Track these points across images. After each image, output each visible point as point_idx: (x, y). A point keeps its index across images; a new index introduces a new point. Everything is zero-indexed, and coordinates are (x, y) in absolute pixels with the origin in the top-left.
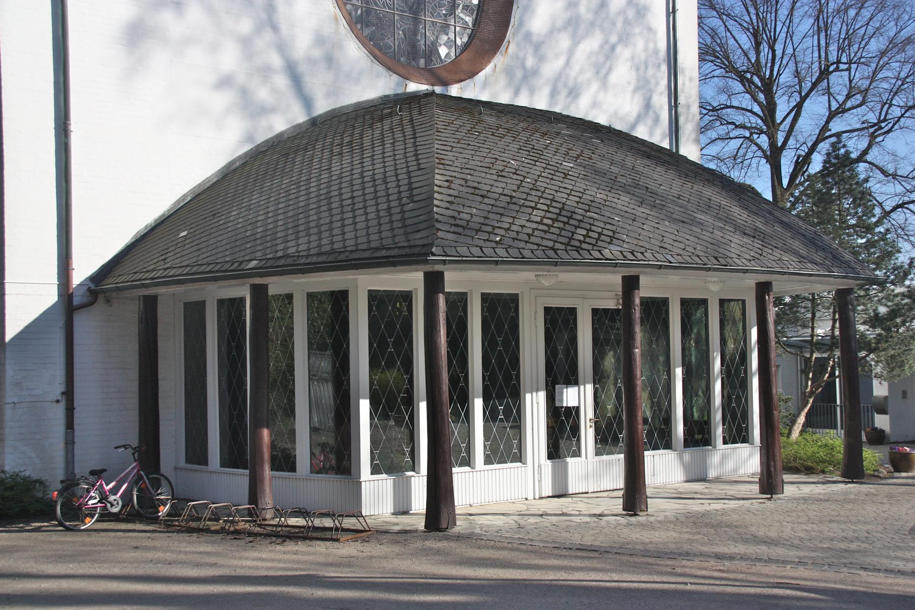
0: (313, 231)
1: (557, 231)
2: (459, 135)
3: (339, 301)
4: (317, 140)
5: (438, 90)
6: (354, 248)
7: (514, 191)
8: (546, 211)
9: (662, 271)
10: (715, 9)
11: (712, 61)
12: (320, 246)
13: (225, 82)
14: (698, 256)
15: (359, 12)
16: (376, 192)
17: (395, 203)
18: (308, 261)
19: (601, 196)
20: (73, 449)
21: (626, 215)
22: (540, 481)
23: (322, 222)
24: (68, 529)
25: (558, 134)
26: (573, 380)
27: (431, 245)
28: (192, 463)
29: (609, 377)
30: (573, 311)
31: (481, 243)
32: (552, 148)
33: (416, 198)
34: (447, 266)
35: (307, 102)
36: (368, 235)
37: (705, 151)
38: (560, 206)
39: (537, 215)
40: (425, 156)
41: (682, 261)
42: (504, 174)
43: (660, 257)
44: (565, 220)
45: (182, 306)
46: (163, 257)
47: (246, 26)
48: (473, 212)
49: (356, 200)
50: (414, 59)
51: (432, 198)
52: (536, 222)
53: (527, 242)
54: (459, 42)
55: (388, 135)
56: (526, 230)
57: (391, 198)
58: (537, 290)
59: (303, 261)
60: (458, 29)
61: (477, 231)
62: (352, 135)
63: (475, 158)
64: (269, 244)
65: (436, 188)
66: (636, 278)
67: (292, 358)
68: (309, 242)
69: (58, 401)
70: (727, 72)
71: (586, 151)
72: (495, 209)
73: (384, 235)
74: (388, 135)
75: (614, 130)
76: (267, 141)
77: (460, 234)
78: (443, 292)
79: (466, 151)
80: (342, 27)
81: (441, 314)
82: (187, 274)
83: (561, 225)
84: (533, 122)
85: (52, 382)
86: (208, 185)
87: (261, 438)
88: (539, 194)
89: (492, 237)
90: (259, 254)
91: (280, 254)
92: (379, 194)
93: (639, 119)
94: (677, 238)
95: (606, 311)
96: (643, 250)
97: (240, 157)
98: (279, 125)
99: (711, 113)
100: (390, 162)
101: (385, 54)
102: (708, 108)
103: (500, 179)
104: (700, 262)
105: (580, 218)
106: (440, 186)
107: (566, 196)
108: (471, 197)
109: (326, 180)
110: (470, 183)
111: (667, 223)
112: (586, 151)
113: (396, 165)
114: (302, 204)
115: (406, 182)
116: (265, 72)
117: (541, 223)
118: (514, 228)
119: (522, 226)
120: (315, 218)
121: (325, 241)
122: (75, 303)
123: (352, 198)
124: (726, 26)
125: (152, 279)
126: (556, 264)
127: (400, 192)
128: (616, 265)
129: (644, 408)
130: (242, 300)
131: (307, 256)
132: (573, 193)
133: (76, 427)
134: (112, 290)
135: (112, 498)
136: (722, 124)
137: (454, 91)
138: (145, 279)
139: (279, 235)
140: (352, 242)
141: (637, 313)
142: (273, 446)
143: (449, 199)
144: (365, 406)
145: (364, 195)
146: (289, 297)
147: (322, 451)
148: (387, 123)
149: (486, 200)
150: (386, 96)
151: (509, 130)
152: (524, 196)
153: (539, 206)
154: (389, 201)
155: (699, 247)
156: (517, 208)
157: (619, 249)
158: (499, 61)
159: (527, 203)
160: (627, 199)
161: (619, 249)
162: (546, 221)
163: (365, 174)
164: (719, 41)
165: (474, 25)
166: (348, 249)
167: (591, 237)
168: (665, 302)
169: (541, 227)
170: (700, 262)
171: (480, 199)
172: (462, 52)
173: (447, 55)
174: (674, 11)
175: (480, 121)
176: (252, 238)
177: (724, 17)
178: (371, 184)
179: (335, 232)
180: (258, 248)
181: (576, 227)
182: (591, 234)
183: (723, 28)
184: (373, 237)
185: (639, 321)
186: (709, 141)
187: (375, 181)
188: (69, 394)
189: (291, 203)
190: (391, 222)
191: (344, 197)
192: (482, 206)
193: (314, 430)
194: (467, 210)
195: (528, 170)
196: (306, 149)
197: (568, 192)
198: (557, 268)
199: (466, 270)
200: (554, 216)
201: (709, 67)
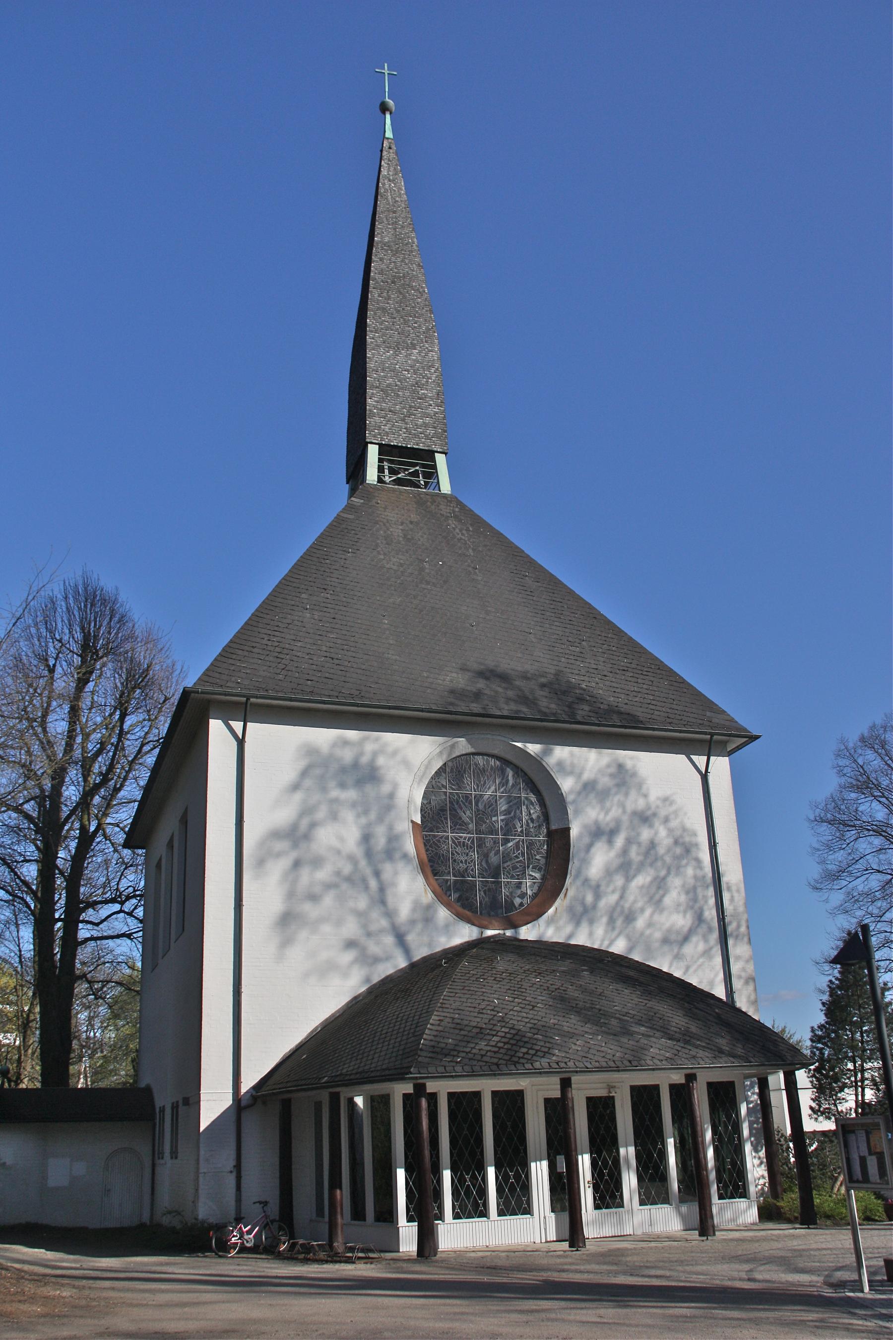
5: (509, 933)
13: (350, 944)
22: (545, 1229)
24: (220, 1257)
27: (411, 1067)
35: (407, 951)
61: (446, 1055)
66: (569, 1079)
69: (231, 1172)
85: (227, 1159)
87: (336, 1196)
98: (386, 969)
135: (246, 1237)
137: (527, 933)
143: (435, 1033)
165: (542, 879)
188: (238, 1167)
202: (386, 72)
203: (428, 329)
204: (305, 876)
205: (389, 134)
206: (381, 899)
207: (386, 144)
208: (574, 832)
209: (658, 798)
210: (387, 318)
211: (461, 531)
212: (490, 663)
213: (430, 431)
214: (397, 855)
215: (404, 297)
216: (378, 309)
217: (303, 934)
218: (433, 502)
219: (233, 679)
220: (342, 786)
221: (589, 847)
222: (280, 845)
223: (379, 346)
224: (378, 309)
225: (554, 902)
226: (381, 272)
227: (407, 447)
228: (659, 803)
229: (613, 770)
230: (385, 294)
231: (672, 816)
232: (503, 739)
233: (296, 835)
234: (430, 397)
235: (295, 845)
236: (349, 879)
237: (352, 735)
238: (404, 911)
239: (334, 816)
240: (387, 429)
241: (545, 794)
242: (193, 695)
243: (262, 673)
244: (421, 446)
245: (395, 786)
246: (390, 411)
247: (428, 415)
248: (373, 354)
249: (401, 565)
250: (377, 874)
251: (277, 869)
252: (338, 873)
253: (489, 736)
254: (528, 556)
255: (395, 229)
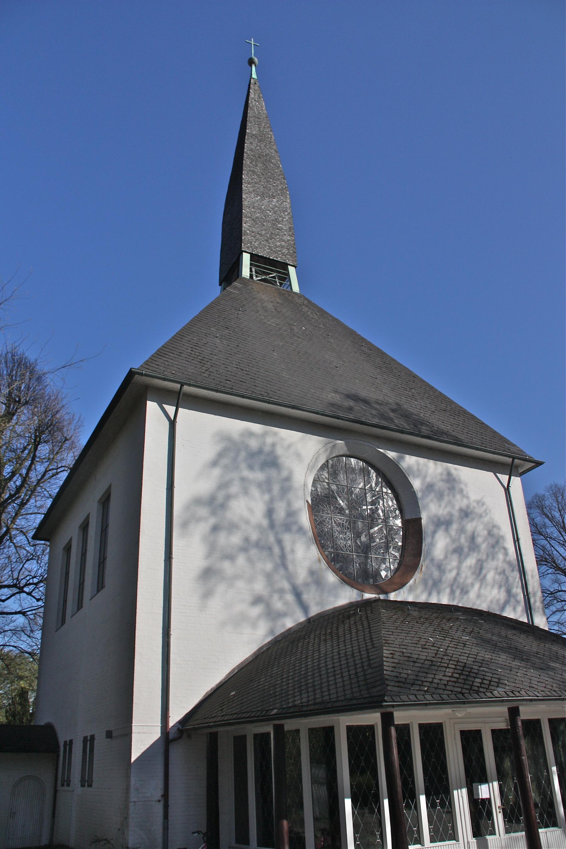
0: (310, 689)
1: (463, 681)
2: (397, 624)
3: (329, 733)
4: (311, 632)
5: (382, 597)
6: (336, 699)
7: (433, 657)
8: (455, 669)
9: (533, 702)
10: (542, 535)
11: (546, 565)
12: (315, 699)
13: (257, 600)
14: (555, 691)
15: (333, 555)
16: (348, 663)
17: (360, 670)
18: (309, 708)
19: (489, 656)
20: (167, 833)
21: (505, 667)
23: (316, 683)
25: (457, 619)
26: (484, 780)
27: (384, 695)
28: (240, 844)
29: (508, 774)
30: (479, 732)
31: (415, 692)
32: (454, 628)
33: (372, 666)
34: (395, 708)
35: (305, 608)
36: (344, 690)
37: (550, 619)
38: (463, 665)
39: (449, 672)
40: (377, 639)
41: (545, 695)
42: (426, 647)
43: (531, 694)
44: (467, 673)
45: (232, 738)
46: (221, 708)
47: (269, 566)
48: (408, 672)
49: (336, 669)
50: (366, 580)
51: (383, 665)
52: (449, 676)
53: (444, 690)
54: (392, 567)
55: (353, 627)
56: (443, 682)
57: (357, 666)
58: (454, 720)
59: (305, 709)
60: (391, 560)
61: (413, 684)
62: (332, 628)
63: (407, 638)
64: (284, 699)
65: (384, 659)
67: (300, 770)
68: (308, 697)
69: (159, 801)
70: (555, 570)
71: (475, 628)
72: (422, 670)
73: (354, 690)
74: (353, 627)
75: (491, 613)
76: (282, 634)
77: (401, 687)
78: (394, 725)
79: (402, 634)
80: (323, 564)
81: (393, 740)
82: (235, 719)
83: (465, 677)
84: (441, 613)
86: (247, 662)
87: (282, 826)
88: (449, 658)
89: (422, 688)
90: (278, 705)
91: (290, 705)
92: (350, 664)
93: (506, 603)
94: (540, 680)
95: (500, 730)
96: (519, 689)
97: (266, 644)
98: (289, 624)
99: (550, 596)
100: (355, 644)
101: (349, 578)
102: (548, 592)
103: (424, 650)
104: (556, 695)
105: (476, 671)
106: (387, 658)
107: (466, 658)
108: (407, 663)
109: (317, 657)
110: (405, 654)
111: (532, 671)
112: (475, 628)
113: (359, 645)
114: (303, 673)
115: (366, 656)
116: (281, 591)
117: (452, 676)
118: (435, 681)
119: (441, 680)
120: (311, 681)
121: (318, 696)
122: (170, 738)
123: (334, 667)
124: (550, 544)
125: (215, 722)
126: (464, 703)
127: (362, 663)
128: (503, 701)
129: (534, 795)
130: (268, 734)
131: (307, 706)
132: (470, 656)
133: (169, 818)
134: (190, 729)
136: (558, 602)
137: (393, 596)
138: (210, 722)
139: (290, 693)
140: (335, 696)
141: (521, 731)
142: (290, 831)
143: (393, 665)
144: (348, 803)
145: (341, 665)
146: (298, 731)
147: (323, 834)
148: (352, 619)
149: (416, 665)
150: (351, 603)
151: (427, 619)
152: (440, 660)
153: (450, 666)
154: (356, 668)
155: (554, 685)
156: (436, 668)
157: (504, 690)
158: (417, 576)
159: (442, 664)
160: (505, 657)
161: (504, 690)
162: (455, 675)
163: (340, 652)
164: (547, 553)
165: (400, 558)
166: (332, 700)
167: (484, 684)
168: (538, 721)
169: (452, 679)
170: (556, 695)
171: (412, 664)
172: (395, 573)
173: (386, 576)
174: (518, 540)
175: (409, 615)
176: (273, 695)
177: (548, 539)
178: (344, 658)
179: (324, 689)
180: (277, 701)
181: (475, 678)
182: (485, 681)
183: (548, 545)
184: (347, 692)
185: (523, 737)
186: (552, 613)
187: (346, 656)
189: (296, 672)
190: (358, 681)
191: (329, 667)
192: (414, 668)
193: (316, 819)
194: (405, 671)
195: (440, 643)
196: (304, 638)
197: (467, 655)
198: (465, 705)
199: (407, 710)
200: (460, 672)
201: (544, 568)
202: (253, 43)
203: (282, 189)
204: (222, 538)
205: (254, 76)
206: (283, 561)
207: (252, 81)
208: (424, 522)
209: (474, 501)
210: (256, 177)
211: (312, 313)
212: (353, 392)
213: (285, 251)
214: (295, 528)
215: (266, 167)
216: (250, 171)
217: (221, 588)
218: (289, 295)
219: (168, 370)
220: (251, 467)
221: (434, 532)
222: (203, 511)
223: (251, 193)
224: (250, 171)
225: (413, 575)
226: (251, 150)
227: (269, 258)
228: (475, 504)
229: (444, 477)
230: (254, 163)
231: (484, 514)
232: (371, 445)
233: (215, 503)
234: (285, 230)
235: (213, 513)
236: (257, 545)
237: (256, 428)
238: (302, 575)
239: (246, 492)
240: (256, 244)
241: (400, 491)
242: (137, 376)
243: (190, 370)
244: (279, 259)
245: (291, 474)
246: (258, 234)
247: (284, 241)
248: (246, 196)
249: (278, 324)
250: (279, 542)
251: (201, 529)
252: (247, 539)
253: (361, 442)
254: (359, 335)
255: (260, 128)
